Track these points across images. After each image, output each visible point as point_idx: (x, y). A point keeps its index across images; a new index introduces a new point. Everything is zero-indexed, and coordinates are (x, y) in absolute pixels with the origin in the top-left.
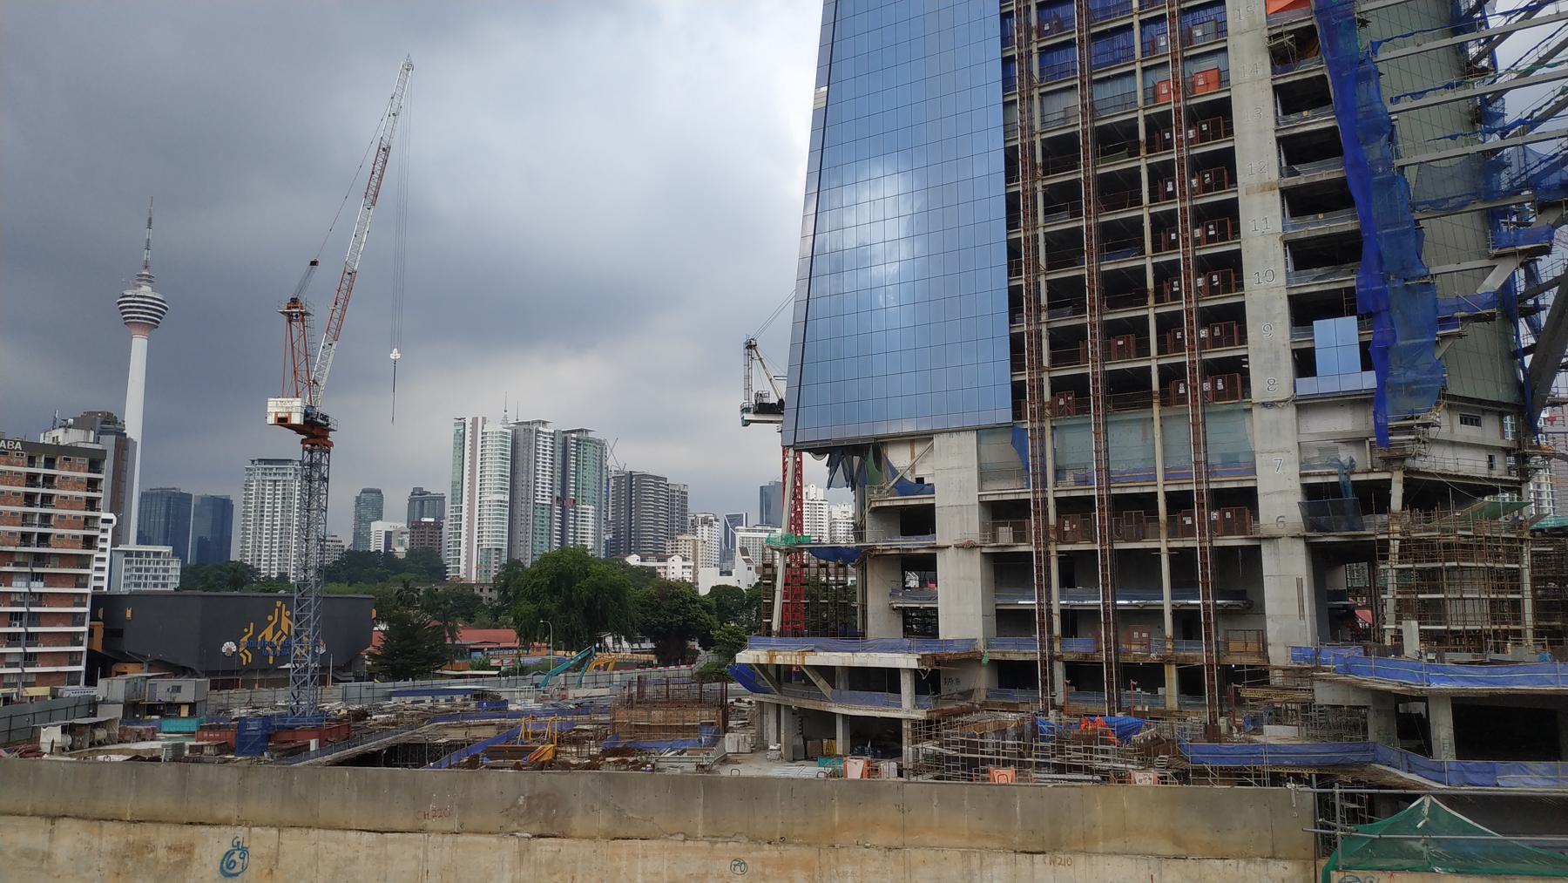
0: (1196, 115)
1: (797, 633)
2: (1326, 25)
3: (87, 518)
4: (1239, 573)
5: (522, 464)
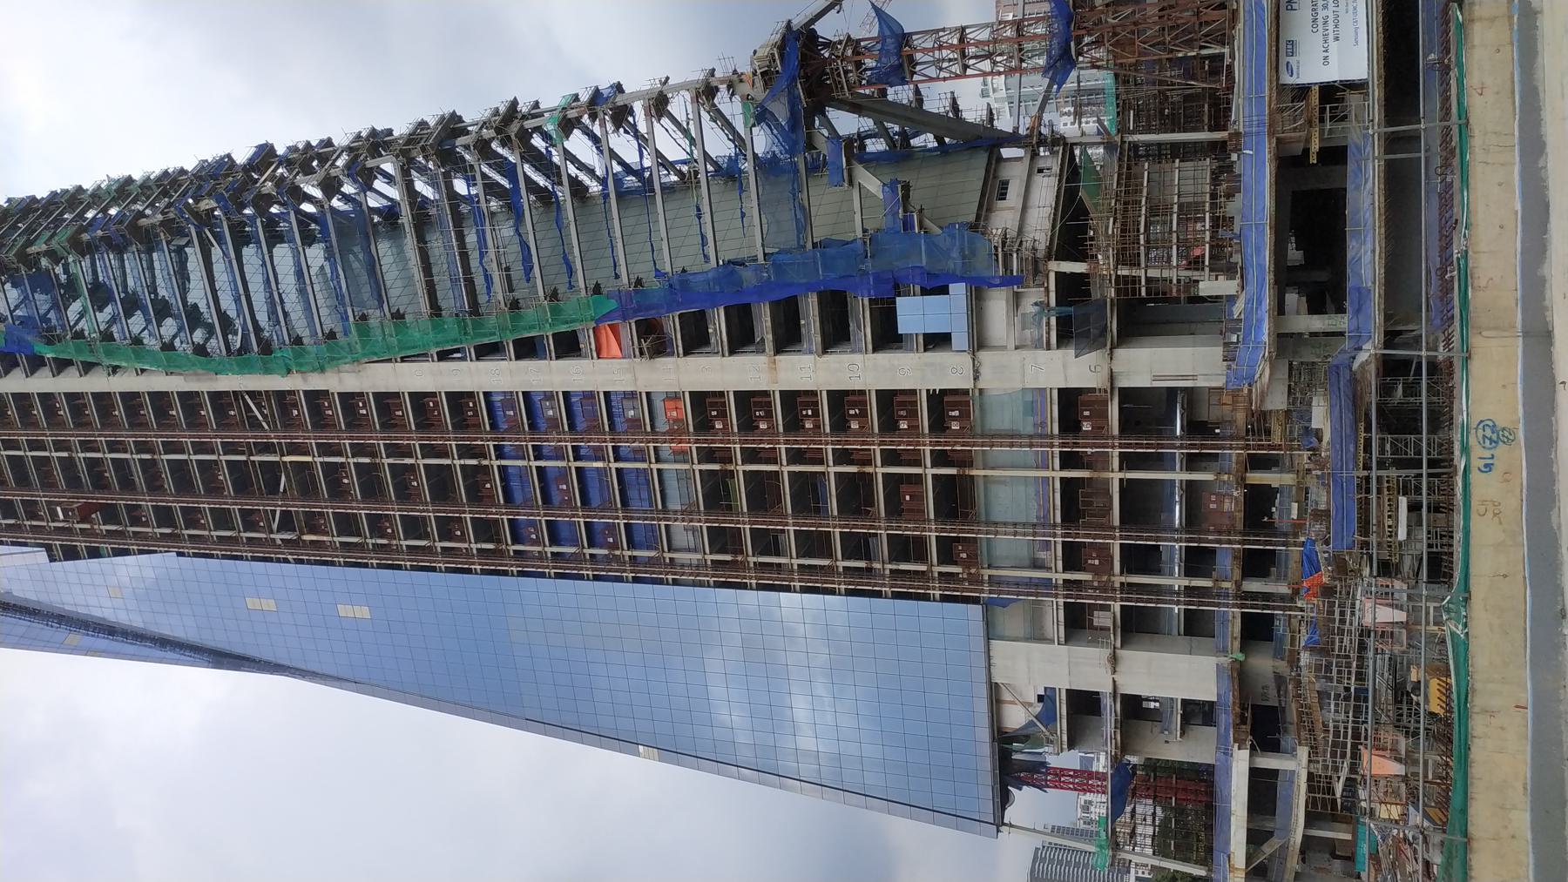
1: (1210, 850)
2: (636, 311)
4: (1145, 411)
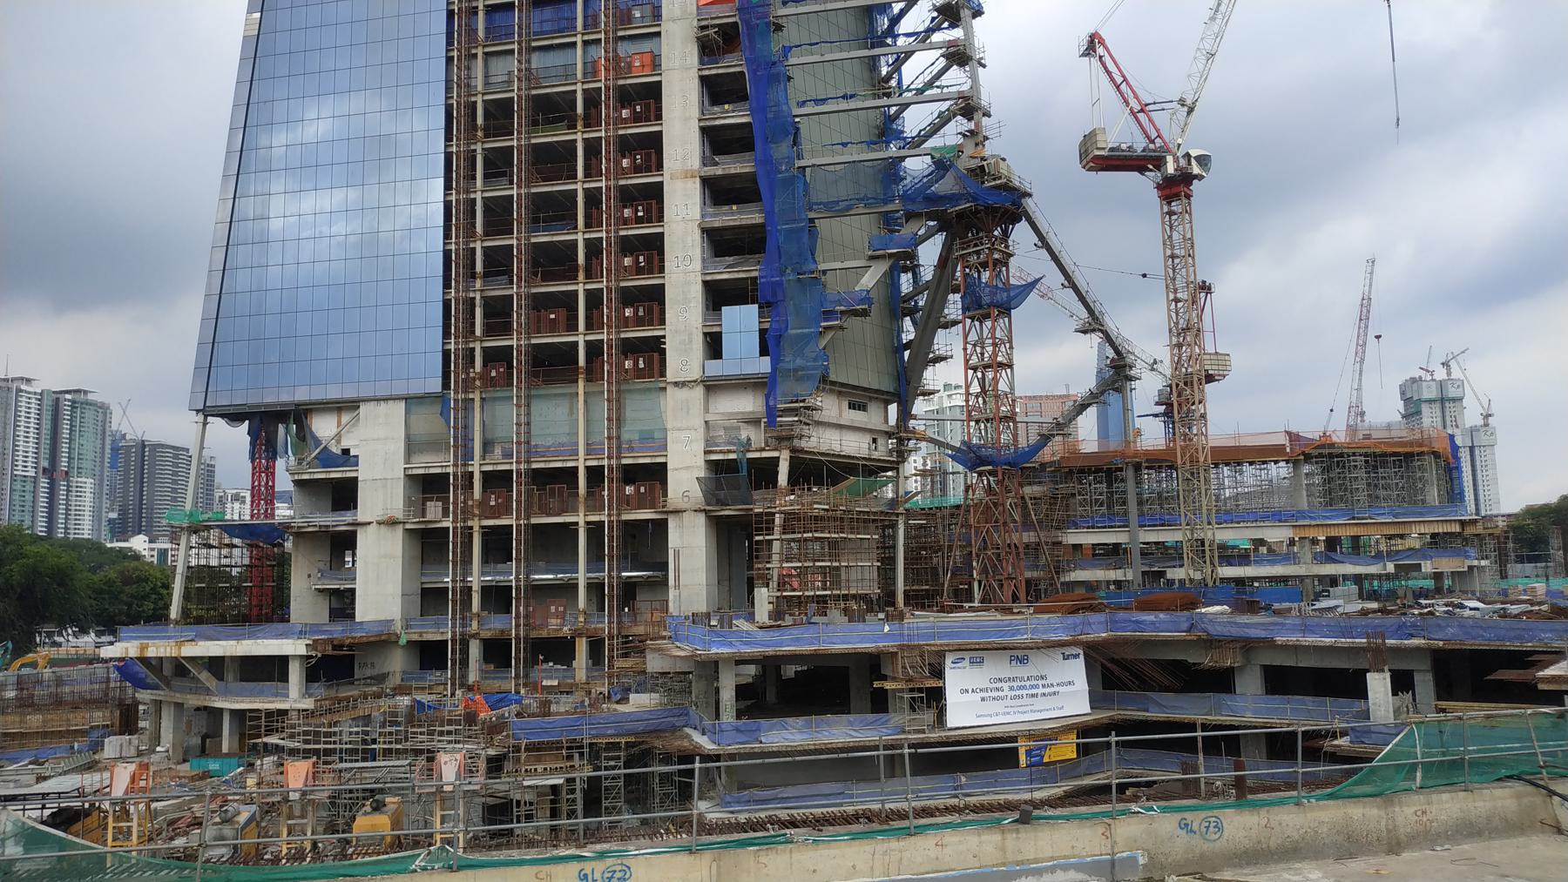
0: (625, 96)
1: (199, 621)
2: (747, 22)
4: (646, 543)
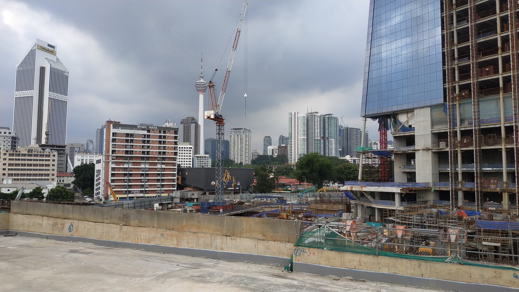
3: (175, 147)
5: (310, 127)
